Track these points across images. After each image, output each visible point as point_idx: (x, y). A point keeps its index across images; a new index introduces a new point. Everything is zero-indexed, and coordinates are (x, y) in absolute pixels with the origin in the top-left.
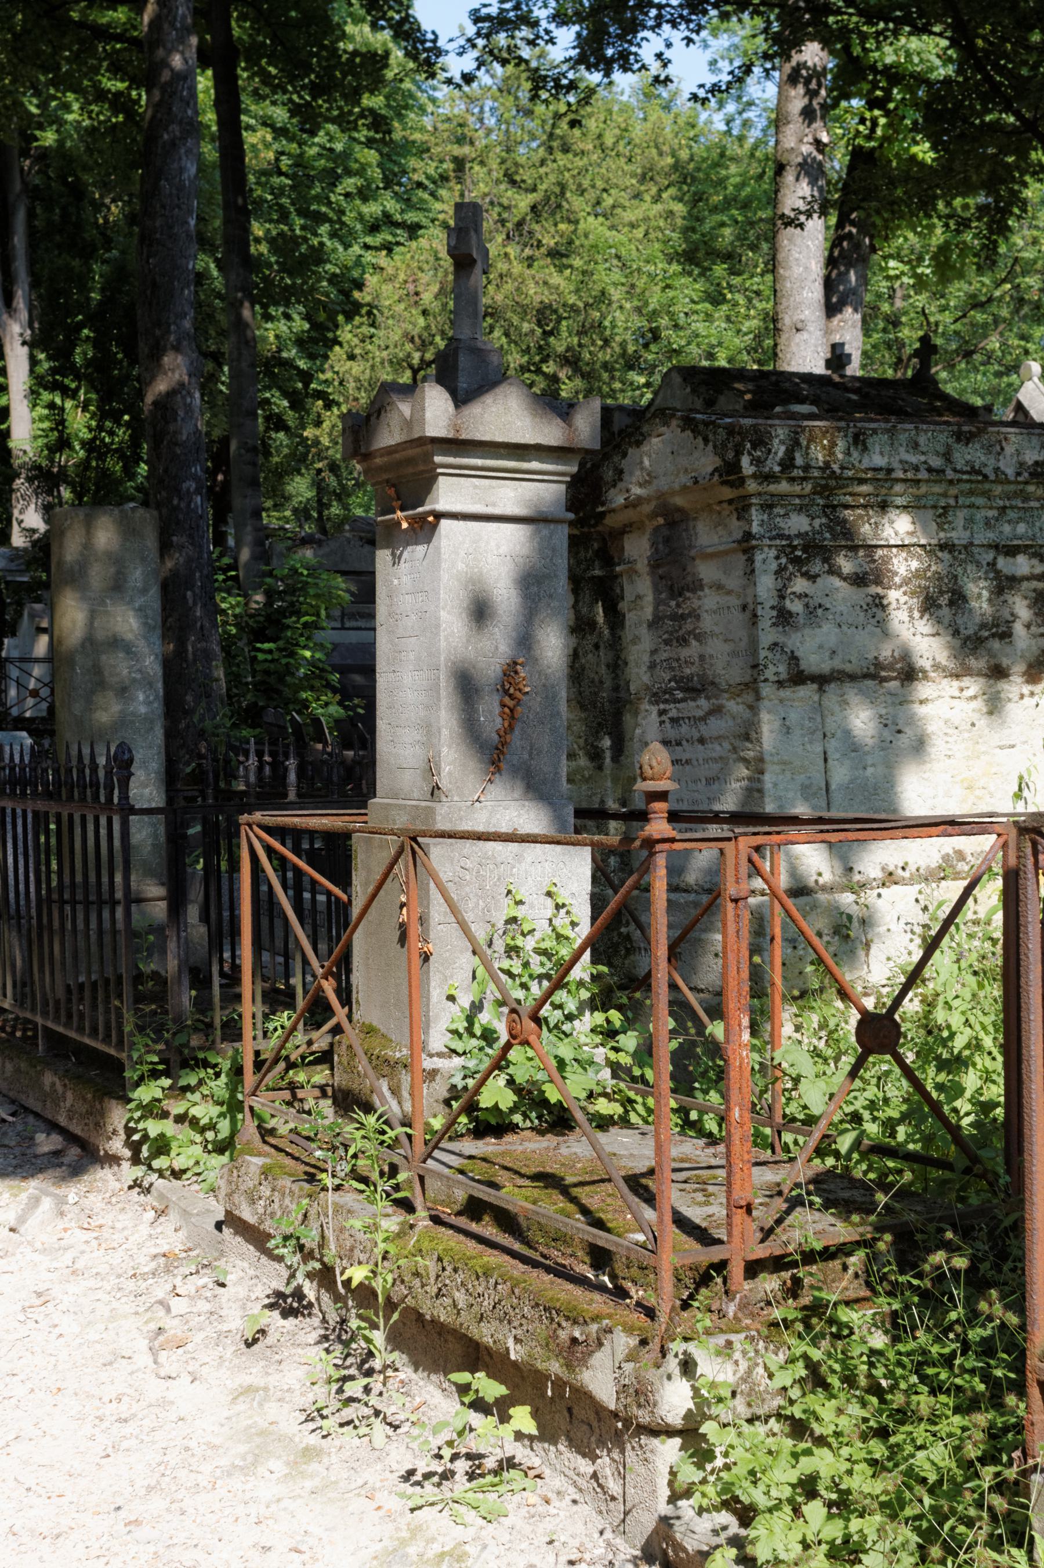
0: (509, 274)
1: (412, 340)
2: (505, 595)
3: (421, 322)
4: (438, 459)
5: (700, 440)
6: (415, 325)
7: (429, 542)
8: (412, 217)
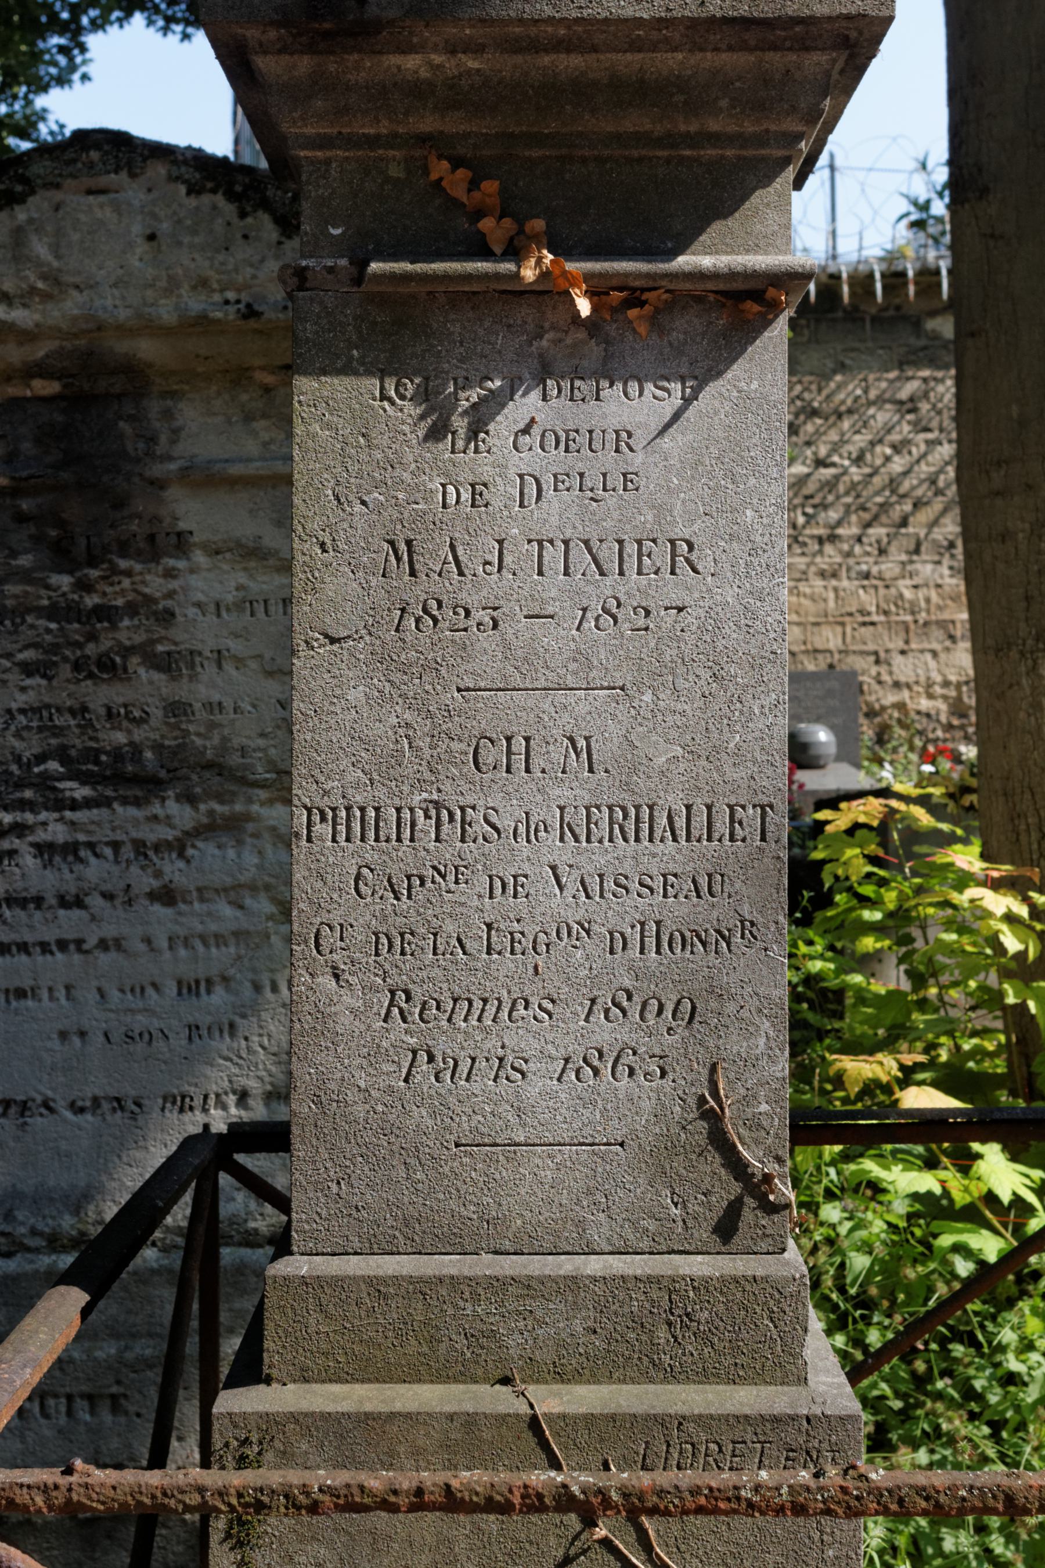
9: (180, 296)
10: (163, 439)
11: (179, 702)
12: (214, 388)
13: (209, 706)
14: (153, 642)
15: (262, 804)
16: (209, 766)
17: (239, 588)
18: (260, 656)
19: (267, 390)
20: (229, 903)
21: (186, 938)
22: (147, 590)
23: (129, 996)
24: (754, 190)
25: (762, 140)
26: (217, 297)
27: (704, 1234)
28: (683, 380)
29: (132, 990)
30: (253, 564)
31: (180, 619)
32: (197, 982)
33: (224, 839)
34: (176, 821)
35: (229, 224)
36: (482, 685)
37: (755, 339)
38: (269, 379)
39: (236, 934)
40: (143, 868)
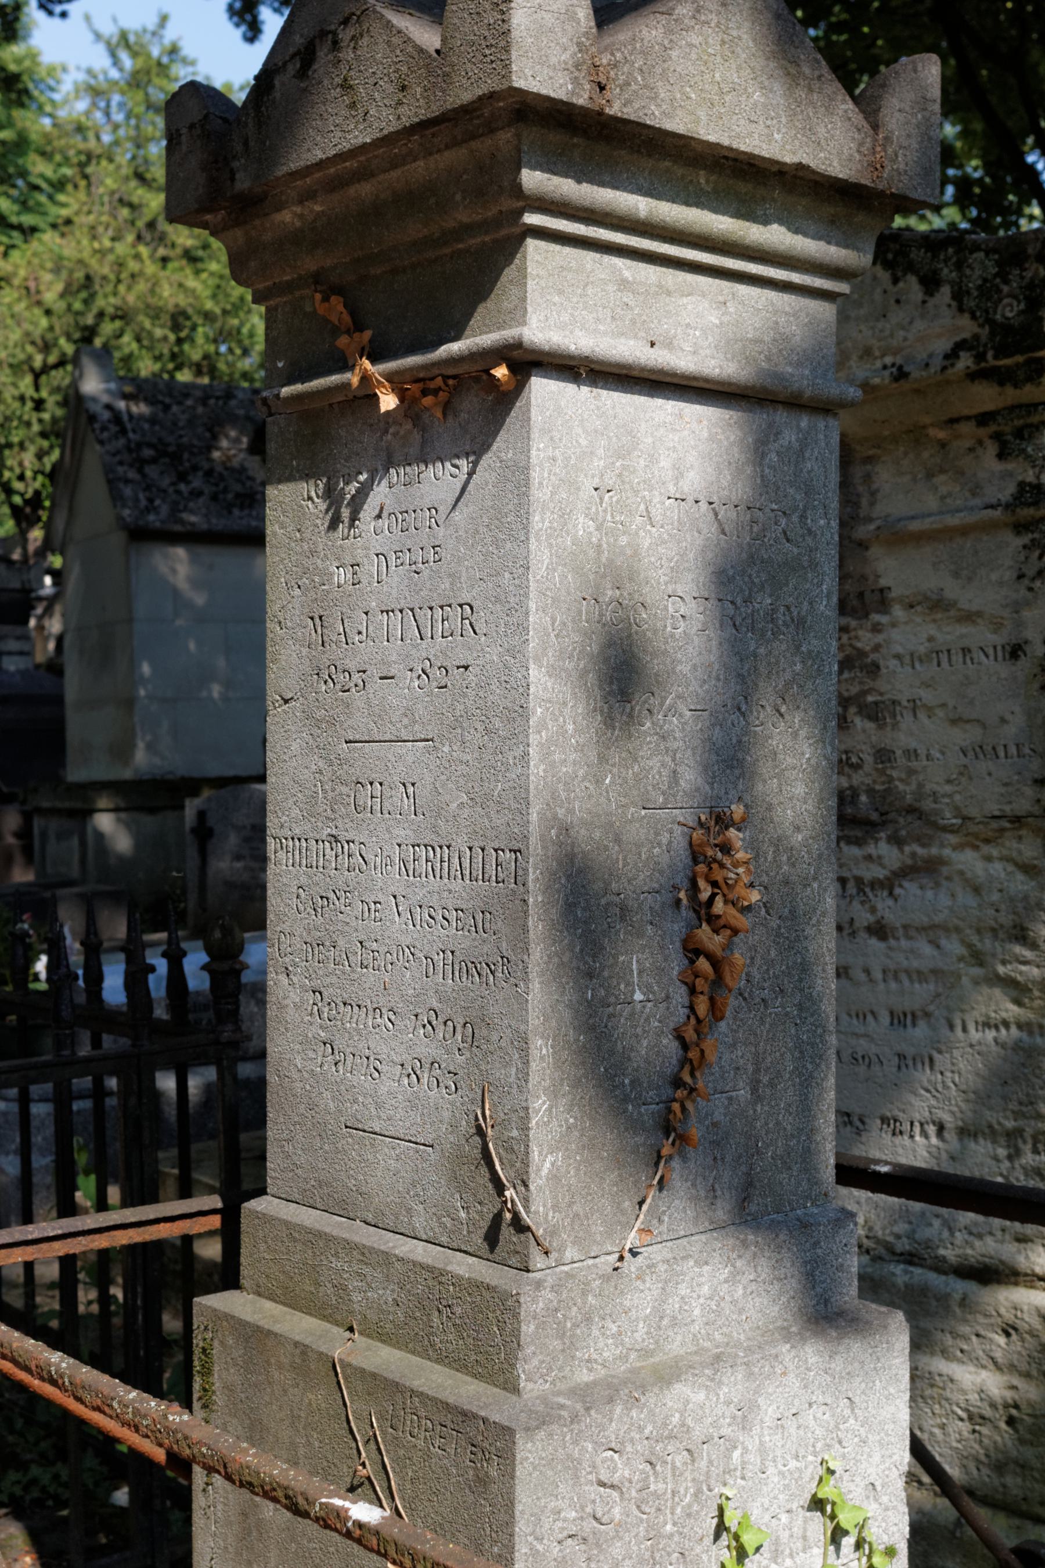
0: (141, 273)
1: (33, 343)
2: (681, 621)
3: (44, 322)
4: (532, 179)
5: (912, 286)
6: (35, 324)
7: (477, 449)
8: (28, 220)
9: (850, 368)
10: (864, 502)
11: (884, 749)
12: (902, 449)
13: (911, 754)
14: (864, 693)
15: (954, 849)
16: (911, 810)
17: (931, 639)
18: (944, 705)
19: (943, 445)
20: (930, 942)
21: (896, 972)
22: (859, 645)
23: (855, 1021)
24: (503, 270)
25: (497, 222)
26: (878, 364)
27: (478, 1240)
28: (467, 455)
29: (857, 1016)
30: (939, 616)
31: (884, 671)
32: (905, 1015)
33: (925, 881)
34: (886, 861)
35: (885, 292)
36: (357, 737)
37: (511, 409)
38: (941, 435)
39: (935, 972)
40: (862, 903)
